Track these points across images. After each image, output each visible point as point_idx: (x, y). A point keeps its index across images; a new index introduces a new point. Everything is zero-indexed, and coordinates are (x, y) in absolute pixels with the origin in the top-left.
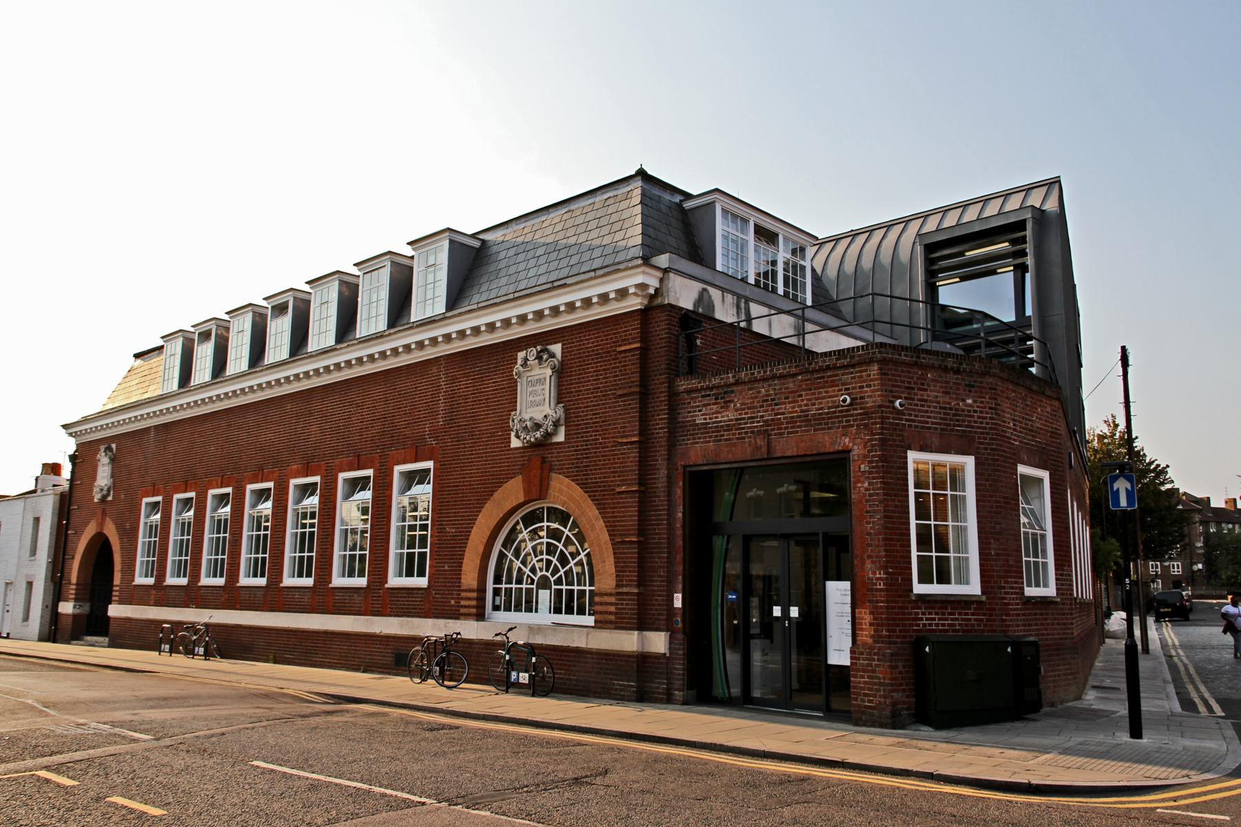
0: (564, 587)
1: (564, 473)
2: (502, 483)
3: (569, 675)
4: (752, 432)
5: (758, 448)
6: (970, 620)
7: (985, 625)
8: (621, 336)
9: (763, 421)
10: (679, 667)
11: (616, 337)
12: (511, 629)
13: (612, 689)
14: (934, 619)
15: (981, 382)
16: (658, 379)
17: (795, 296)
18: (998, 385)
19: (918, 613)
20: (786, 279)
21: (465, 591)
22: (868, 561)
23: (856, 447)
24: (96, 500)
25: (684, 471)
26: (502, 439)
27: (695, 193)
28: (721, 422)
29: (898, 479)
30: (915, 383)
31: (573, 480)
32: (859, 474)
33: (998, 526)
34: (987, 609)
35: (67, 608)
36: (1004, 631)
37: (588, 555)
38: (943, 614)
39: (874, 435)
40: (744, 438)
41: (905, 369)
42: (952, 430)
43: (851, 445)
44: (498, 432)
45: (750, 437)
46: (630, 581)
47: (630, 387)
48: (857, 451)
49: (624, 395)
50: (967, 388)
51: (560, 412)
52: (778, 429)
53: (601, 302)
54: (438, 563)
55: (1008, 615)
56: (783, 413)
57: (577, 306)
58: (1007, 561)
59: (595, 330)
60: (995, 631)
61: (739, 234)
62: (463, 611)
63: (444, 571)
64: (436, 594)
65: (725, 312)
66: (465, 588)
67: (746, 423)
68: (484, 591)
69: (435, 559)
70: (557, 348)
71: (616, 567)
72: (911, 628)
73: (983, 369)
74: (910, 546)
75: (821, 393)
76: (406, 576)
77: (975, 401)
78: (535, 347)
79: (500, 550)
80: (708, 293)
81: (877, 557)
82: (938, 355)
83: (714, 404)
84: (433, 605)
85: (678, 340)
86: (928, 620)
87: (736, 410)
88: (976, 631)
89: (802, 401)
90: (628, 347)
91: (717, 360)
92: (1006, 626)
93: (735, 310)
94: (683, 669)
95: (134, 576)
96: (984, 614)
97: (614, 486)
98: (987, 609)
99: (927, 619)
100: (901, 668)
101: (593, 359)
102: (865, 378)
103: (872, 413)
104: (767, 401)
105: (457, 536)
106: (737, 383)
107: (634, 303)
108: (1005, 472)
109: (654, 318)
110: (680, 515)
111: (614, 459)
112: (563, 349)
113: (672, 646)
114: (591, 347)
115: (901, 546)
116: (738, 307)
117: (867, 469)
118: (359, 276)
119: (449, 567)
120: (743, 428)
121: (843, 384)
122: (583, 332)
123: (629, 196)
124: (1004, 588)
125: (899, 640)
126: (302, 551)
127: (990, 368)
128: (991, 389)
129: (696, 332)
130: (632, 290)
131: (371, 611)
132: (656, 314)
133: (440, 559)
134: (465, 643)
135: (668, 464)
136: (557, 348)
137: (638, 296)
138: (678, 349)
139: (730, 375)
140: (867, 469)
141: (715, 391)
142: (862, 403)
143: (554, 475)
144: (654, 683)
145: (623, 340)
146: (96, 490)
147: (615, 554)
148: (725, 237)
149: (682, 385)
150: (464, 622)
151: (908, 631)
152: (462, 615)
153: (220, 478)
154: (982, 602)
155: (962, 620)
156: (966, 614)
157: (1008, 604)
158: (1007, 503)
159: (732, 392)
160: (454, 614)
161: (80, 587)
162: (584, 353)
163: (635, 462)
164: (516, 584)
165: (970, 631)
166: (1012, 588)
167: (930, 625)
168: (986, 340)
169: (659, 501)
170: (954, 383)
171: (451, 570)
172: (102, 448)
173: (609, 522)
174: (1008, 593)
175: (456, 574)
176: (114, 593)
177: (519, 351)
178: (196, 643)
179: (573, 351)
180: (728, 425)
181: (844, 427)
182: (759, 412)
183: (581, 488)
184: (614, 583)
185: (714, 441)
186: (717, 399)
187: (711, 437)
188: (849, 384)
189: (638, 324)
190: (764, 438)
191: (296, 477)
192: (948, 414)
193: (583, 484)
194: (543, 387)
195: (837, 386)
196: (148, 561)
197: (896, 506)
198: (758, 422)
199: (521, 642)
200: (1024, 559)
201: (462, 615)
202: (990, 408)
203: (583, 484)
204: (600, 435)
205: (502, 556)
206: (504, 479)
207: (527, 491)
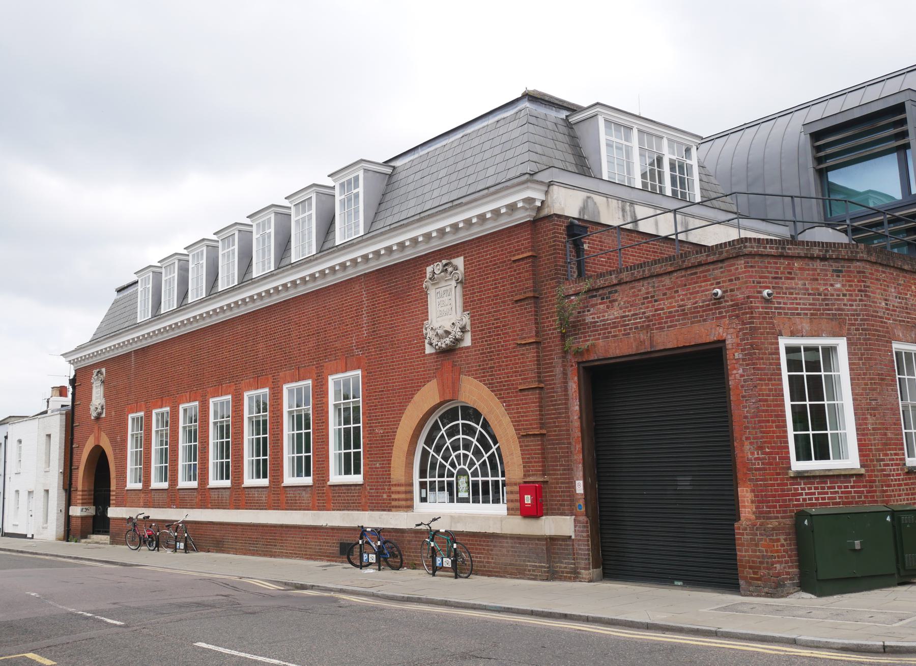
0: (480, 479)
1: (473, 375)
2: (420, 386)
3: (488, 558)
4: (636, 328)
5: (642, 342)
6: (850, 492)
7: (866, 497)
8: (514, 247)
9: (645, 317)
10: (584, 549)
11: (510, 248)
12: (434, 520)
13: (525, 570)
14: (814, 494)
15: (849, 267)
16: (549, 284)
17: (683, 194)
18: (866, 268)
19: (797, 489)
20: (673, 179)
21: (395, 485)
22: (747, 443)
23: (729, 337)
24: (93, 418)
25: (578, 367)
26: (417, 347)
27: (585, 105)
28: (607, 320)
29: (771, 364)
30: (782, 273)
31: (481, 381)
32: (734, 362)
33: (874, 403)
34: (867, 481)
35: (76, 511)
36: (887, 502)
37: (498, 449)
38: (823, 488)
39: (745, 324)
40: (629, 334)
41: (771, 261)
42: (823, 314)
43: (725, 334)
44: (414, 340)
45: (635, 333)
46: (536, 471)
47: (525, 293)
48: (730, 341)
49: (520, 300)
50: (835, 274)
51: (466, 320)
52: (659, 324)
53: (510, 212)
54: (371, 461)
55: (889, 486)
56: (663, 309)
57: (433, 236)
58: (885, 434)
59: (492, 242)
60: (876, 502)
61: (623, 142)
62: (394, 503)
63: (376, 468)
64: (371, 489)
65: (611, 215)
66: (394, 483)
67: (630, 320)
68: (411, 485)
69: (368, 458)
70: (459, 262)
71: (523, 458)
72: (791, 503)
73: (850, 254)
74: (785, 426)
75: (695, 288)
76: (345, 474)
77: (843, 285)
78: (441, 261)
79: (424, 448)
80: (593, 201)
81: (754, 438)
82: (803, 245)
83: (601, 304)
84: (369, 499)
85: (565, 246)
86: (807, 495)
87: (621, 309)
88: (857, 503)
89: (679, 296)
90: (521, 256)
91: (606, 262)
92: (887, 496)
93: (621, 214)
94: (588, 550)
95: (126, 482)
96: (865, 486)
97: (517, 384)
98: (867, 481)
99: (807, 494)
100: (783, 541)
101: (491, 269)
102: (733, 271)
103: (742, 304)
104: (647, 298)
105: (385, 436)
106: (620, 283)
107: (522, 216)
108: (878, 350)
109: (542, 228)
110: (577, 408)
111: (515, 360)
112: (465, 261)
113: (577, 529)
114: (489, 258)
115: (777, 427)
116: (623, 210)
117: (741, 356)
118: (333, 188)
119: (380, 464)
120: (628, 325)
121: (715, 279)
122: (481, 245)
123: (517, 117)
124: (883, 460)
125: (779, 515)
126: (258, 455)
127: (857, 253)
128: (859, 272)
129: (582, 238)
130: (520, 205)
131: (318, 506)
132: (544, 224)
133: (371, 458)
134: (398, 532)
135: (563, 361)
136: (459, 262)
137: (526, 209)
138: (566, 255)
139: (613, 276)
140: (741, 356)
141: (601, 292)
142: (732, 296)
143: (463, 377)
144: (562, 563)
145: (516, 250)
146: (92, 408)
147: (521, 446)
148: (609, 145)
149: (571, 288)
150: (395, 513)
151: (789, 506)
152: (393, 507)
153: (189, 393)
154: (861, 475)
155: (842, 492)
156: (846, 487)
157: (889, 475)
158: (882, 379)
159: (616, 291)
160: (387, 507)
161: (85, 493)
162: (483, 264)
163: (534, 361)
164: (439, 477)
165: (851, 503)
166: (893, 460)
167: (811, 499)
168: (852, 226)
170: (821, 270)
171: (381, 468)
172: (95, 372)
173: (514, 417)
174: (888, 465)
175: (386, 471)
176: (111, 498)
177: (427, 266)
178: (176, 540)
179: (474, 263)
181: (717, 318)
182: (641, 308)
183: (489, 388)
184: (521, 474)
186: (602, 299)
187: (600, 334)
188: (720, 278)
189: (528, 235)
190: (647, 332)
192: (818, 300)
193: (490, 384)
194: (450, 297)
195: (709, 280)
196: (136, 469)
197: (770, 390)
198: (641, 318)
199: (442, 530)
200: (904, 431)
201: (393, 507)
202: (859, 291)
203: (490, 384)
204: (502, 338)
205: (425, 453)
206: (421, 382)
207: (442, 392)
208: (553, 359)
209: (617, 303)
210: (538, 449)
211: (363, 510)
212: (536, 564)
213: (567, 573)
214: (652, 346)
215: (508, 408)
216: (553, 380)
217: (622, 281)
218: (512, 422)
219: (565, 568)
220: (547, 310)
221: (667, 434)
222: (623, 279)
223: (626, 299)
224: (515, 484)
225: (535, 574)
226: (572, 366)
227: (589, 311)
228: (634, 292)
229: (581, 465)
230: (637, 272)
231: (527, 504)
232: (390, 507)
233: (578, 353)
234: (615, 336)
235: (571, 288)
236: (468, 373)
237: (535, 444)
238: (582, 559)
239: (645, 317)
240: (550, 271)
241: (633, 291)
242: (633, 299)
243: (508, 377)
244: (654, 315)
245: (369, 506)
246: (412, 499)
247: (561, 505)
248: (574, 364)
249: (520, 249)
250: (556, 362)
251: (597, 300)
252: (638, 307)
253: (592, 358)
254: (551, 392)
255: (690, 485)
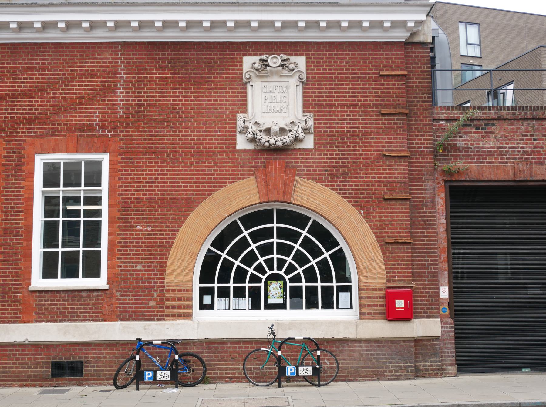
9: (524, 151)
10: (450, 347)
16: (421, 105)
28: (482, 148)
62: (168, 311)
71: (385, 265)
83: (475, 133)
87: (498, 140)
104: (526, 136)
106: (499, 119)
107: (400, 35)
109: (414, 53)
110: (444, 221)
132: (417, 49)
141: (475, 123)
144: (427, 361)
147: (383, 253)
149: (443, 114)
152: (168, 315)
159: (493, 125)
169: (426, 209)
180: (490, 151)
185: (476, 163)
190: (527, 164)
191: (110, 161)
201: (168, 315)
208: (423, 174)
209: (494, 135)
210: (408, 257)
211: (105, 321)
212: (400, 365)
213: (432, 370)
214: (531, 176)
215: (367, 216)
216: (422, 194)
217: (502, 117)
218: (372, 229)
219: (431, 365)
220: (416, 128)
221: (518, 249)
222: (503, 116)
223: (504, 133)
224: (380, 289)
225: (399, 374)
226: (439, 183)
227: (461, 137)
228: (513, 129)
229: (446, 273)
230: (519, 112)
231: (398, 308)
232: (162, 315)
233: (448, 172)
234: (490, 163)
235: (443, 114)
236: (309, 176)
237: (401, 252)
238: (449, 356)
239: (524, 151)
240: (423, 94)
241: (511, 127)
242: (512, 134)
243: (368, 185)
244: (533, 151)
245: (118, 316)
246: (191, 307)
247: (428, 308)
248: (441, 182)
249: (391, 66)
250: (427, 177)
251: (471, 129)
252: (516, 142)
253: (463, 179)
254: (420, 205)
255: (541, 290)
